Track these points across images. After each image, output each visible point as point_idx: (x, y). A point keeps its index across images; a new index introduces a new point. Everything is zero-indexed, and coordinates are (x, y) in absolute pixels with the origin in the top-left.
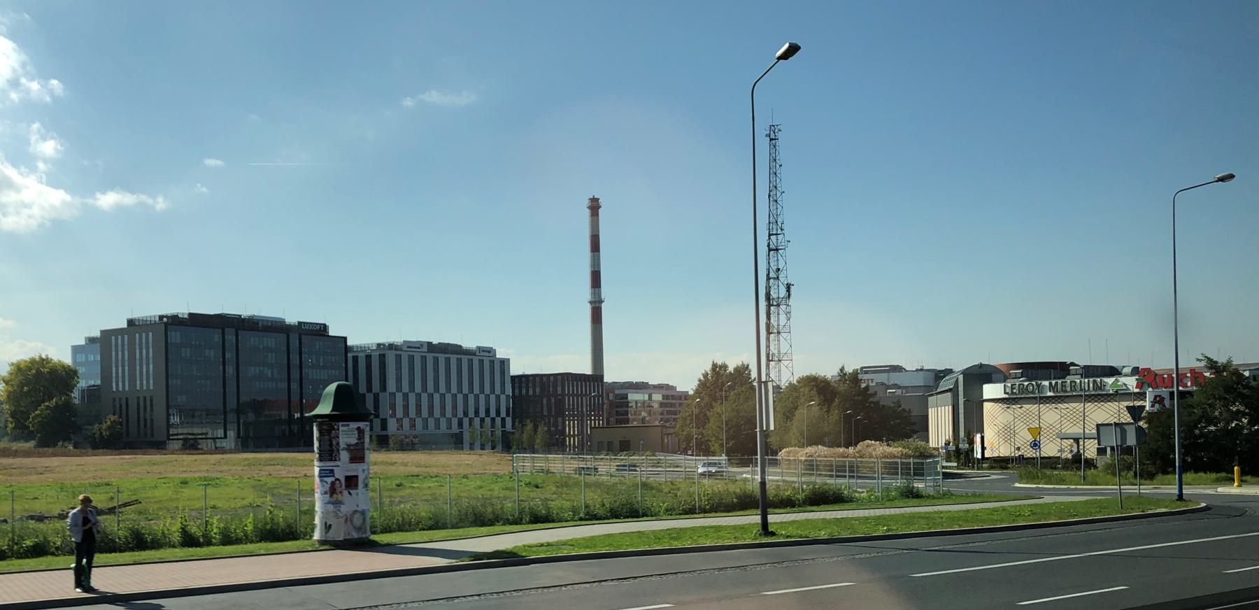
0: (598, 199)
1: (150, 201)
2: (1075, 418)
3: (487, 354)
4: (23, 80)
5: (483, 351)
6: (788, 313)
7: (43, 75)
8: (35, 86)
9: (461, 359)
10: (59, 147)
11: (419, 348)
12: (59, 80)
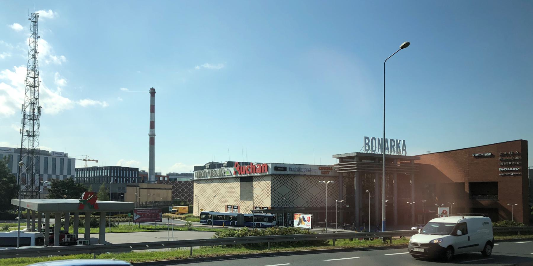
0: (155, 89)
1: (101, 103)
4: (51, 56)
5: (56, 154)
6: (39, 124)
8: (55, 58)
11: (7, 151)
12: (64, 56)
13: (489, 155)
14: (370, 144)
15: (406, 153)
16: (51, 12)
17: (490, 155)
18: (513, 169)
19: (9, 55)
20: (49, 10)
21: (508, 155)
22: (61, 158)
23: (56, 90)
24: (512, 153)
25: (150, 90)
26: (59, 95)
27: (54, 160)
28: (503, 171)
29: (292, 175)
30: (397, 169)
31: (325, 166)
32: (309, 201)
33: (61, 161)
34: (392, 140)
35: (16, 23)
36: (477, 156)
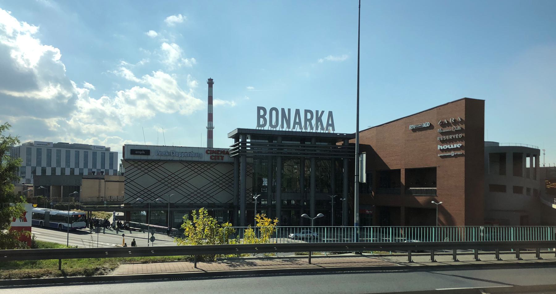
0: (213, 80)
2: (199, 195)
3: (101, 149)
4: (183, 59)
7: (189, 57)
8: (186, 61)
9: (105, 153)
10: (197, 83)
11: (46, 145)
13: (428, 125)
14: (267, 117)
15: (334, 130)
16: (180, 16)
17: (428, 126)
18: (454, 146)
19: (148, 61)
20: (179, 15)
21: (449, 124)
22: (102, 152)
23: (189, 91)
24: (453, 121)
25: (208, 80)
26: (192, 96)
27: (95, 154)
28: (442, 150)
29: (159, 161)
30: (315, 152)
31: (217, 150)
32: (189, 195)
33: (85, 155)
34: (306, 111)
35: (151, 30)
36: (414, 128)
